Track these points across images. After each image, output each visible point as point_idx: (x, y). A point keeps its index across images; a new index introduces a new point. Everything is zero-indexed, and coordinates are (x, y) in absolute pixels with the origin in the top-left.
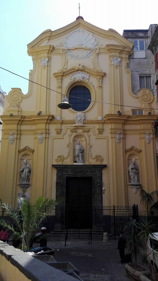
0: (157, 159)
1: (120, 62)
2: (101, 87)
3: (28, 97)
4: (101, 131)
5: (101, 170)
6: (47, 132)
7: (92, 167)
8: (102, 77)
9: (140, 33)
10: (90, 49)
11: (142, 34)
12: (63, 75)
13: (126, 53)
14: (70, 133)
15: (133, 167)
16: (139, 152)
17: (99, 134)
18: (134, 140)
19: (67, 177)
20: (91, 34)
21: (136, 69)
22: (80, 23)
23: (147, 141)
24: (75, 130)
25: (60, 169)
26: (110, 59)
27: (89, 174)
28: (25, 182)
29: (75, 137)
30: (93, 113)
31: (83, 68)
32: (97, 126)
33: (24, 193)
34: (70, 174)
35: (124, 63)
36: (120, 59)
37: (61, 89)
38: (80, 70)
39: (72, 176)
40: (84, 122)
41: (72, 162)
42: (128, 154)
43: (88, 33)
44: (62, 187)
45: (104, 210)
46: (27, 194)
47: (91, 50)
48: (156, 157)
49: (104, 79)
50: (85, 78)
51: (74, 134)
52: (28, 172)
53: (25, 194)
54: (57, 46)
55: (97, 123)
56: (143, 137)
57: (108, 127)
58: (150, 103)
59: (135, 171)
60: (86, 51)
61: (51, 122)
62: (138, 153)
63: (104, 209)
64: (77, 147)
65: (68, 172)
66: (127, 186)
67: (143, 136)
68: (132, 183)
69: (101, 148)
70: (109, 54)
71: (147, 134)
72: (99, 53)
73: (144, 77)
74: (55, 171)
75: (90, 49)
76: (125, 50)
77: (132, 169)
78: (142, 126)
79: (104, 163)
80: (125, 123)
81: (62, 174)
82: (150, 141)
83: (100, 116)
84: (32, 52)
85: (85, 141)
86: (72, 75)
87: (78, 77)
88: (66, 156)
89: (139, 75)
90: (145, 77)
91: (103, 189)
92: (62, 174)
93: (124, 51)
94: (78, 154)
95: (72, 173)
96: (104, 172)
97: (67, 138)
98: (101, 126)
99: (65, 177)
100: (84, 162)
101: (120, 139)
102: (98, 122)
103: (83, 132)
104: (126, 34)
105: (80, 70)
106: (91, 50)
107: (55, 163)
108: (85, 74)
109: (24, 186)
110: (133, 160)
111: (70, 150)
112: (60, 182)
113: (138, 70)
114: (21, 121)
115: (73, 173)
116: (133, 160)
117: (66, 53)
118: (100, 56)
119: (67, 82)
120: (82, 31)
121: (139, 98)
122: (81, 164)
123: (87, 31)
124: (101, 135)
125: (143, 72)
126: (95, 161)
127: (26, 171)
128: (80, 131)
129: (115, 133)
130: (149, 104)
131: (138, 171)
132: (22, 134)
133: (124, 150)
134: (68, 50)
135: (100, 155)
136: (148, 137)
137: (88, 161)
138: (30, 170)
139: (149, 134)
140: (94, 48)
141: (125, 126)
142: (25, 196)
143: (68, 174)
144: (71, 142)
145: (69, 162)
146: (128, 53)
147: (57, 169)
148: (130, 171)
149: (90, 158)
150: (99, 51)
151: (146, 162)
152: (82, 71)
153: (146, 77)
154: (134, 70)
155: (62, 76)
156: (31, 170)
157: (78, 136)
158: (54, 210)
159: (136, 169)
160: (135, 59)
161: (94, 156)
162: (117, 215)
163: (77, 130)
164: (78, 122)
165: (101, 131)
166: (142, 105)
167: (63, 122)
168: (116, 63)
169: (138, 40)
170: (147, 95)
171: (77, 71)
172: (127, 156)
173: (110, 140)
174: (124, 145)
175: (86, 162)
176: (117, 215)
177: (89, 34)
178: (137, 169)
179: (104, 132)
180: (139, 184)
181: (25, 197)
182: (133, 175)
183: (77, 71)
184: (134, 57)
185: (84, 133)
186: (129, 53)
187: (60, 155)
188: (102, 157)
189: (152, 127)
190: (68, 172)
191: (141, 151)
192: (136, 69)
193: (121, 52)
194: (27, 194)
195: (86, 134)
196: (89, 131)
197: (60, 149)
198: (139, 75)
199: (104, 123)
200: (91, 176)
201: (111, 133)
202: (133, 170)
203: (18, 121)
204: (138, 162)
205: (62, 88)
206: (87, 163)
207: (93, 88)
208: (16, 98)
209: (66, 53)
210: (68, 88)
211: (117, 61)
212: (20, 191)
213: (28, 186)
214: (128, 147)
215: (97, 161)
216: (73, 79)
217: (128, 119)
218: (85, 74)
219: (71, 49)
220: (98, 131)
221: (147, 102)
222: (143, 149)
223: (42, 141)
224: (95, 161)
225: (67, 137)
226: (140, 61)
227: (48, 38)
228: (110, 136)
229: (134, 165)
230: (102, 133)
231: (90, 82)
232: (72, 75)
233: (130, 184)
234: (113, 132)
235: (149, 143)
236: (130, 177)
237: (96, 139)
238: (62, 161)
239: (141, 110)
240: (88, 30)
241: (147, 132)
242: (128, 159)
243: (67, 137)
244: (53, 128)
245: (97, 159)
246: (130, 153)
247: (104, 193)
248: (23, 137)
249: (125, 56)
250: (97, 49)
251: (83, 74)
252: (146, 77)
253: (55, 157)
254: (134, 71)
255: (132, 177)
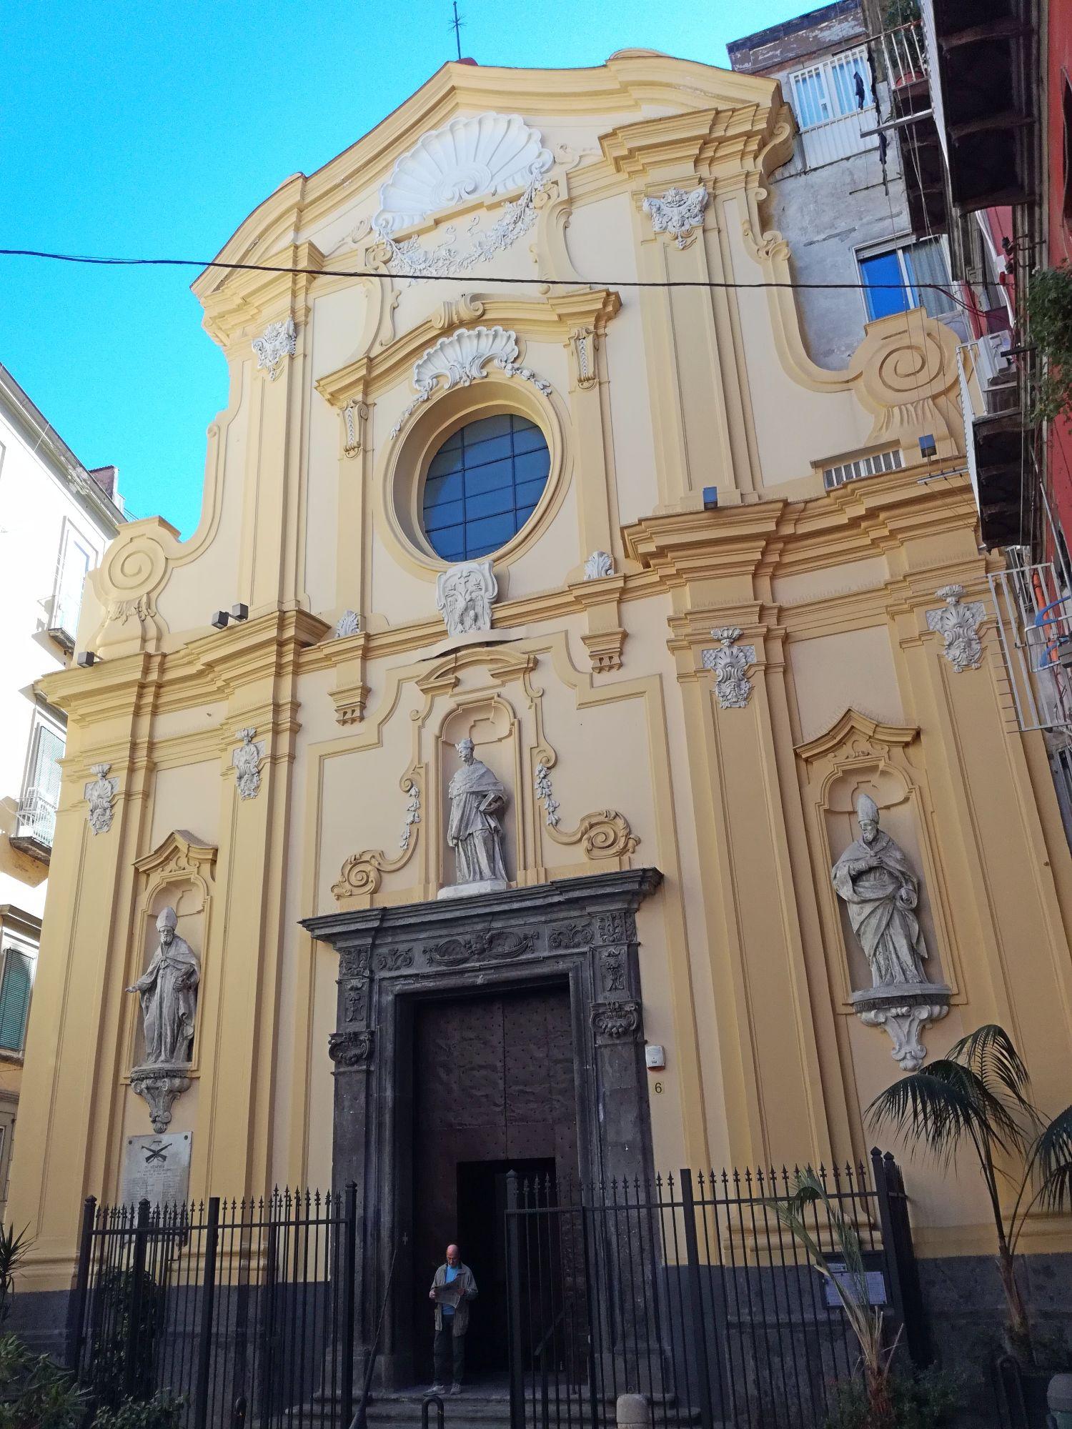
0: (1054, 773)
1: (705, 208)
2: (594, 380)
3: (195, 555)
4: (610, 653)
5: (629, 914)
6: (287, 720)
7: (556, 899)
8: (598, 319)
9: (829, 28)
10: (518, 197)
11: (845, 25)
12: (371, 374)
13: (740, 146)
14: (421, 701)
15: (862, 865)
16: (907, 745)
17: (601, 670)
18: (852, 671)
19: (401, 997)
20: (518, 119)
21: (832, 226)
22: (453, 88)
23: (955, 652)
24: (450, 679)
25: (362, 937)
26: (639, 208)
27: (544, 956)
28: (162, 1057)
29: (451, 720)
30: (559, 547)
31: (478, 304)
32: (581, 623)
33: (161, 1131)
34: (419, 968)
35: (736, 213)
36: (697, 195)
37: (361, 457)
38: (462, 324)
39: (430, 984)
40: (498, 615)
41: (433, 885)
42: (824, 769)
43: (504, 118)
44: (368, 1072)
45: (667, 1210)
46: (174, 1140)
47: (523, 201)
48: (1050, 757)
49: (615, 329)
50: (496, 362)
51: (445, 703)
52: (178, 990)
53: (166, 1139)
54: (342, 243)
55: (578, 599)
56: (692, 668)
57: (652, 616)
58: (946, 392)
59: (880, 894)
60: (498, 212)
61: (304, 659)
62: (898, 751)
63: (666, 1200)
64: (460, 783)
65: (409, 962)
66: (835, 1014)
67: (914, 622)
68: (877, 989)
69: (619, 756)
70: (639, 183)
71: (942, 599)
72: (571, 201)
73: (894, 252)
74: (330, 962)
75: (518, 197)
76: (730, 133)
77: (856, 878)
78: (905, 557)
79: (642, 860)
80: (778, 565)
81: (372, 980)
82: (976, 646)
83: (595, 554)
84: (222, 316)
85: (511, 738)
86: (419, 366)
87: (453, 363)
88: (395, 852)
89: (857, 251)
90: (900, 252)
91: (651, 1056)
92: (372, 980)
93: (722, 141)
94: (465, 822)
95: (431, 961)
96: (652, 926)
97: (405, 735)
98: (605, 617)
99: (390, 998)
100: (510, 877)
101: (745, 676)
102: (579, 597)
103: (498, 682)
104: (745, 59)
105: (462, 324)
106: (523, 201)
107: (329, 906)
108: (495, 336)
109: (149, 1082)
110: (863, 806)
111: (422, 812)
112: (356, 1034)
113: (842, 225)
114: (153, 689)
115: (439, 964)
116: (863, 806)
117: (390, 260)
118: (580, 215)
119: (398, 403)
120: (466, 125)
121: (860, 382)
122: (483, 891)
123: (493, 114)
124: (614, 675)
125: (877, 228)
126: (580, 851)
127: (167, 983)
128: (477, 678)
129: (695, 641)
130: (934, 397)
131: (919, 888)
132: (162, 766)
133: (131, 858)
134: (397, 241)
135: (614, 807)
136: (953, 620)
137: (540, 861)
138: (191, 973)
139: (959, 598)
140: (537, 185)
141: (781, 584)
142: (163, 1153)
143: (406, 977)
144: (429, 755)
145: (409, 888)
146: (753, 146)
147: (339, 950)
148: (846, 892)
149: (546, 837)
150: (569, 189)
151: (969, 808)
152: (473, 323)
153: (905, 249)
154: (818, 233)
155: (367, 384)
156: (199, 975)
157: (467, 712)
158: (322, 1227)
159: (903, 888)
160: (815, 169)
161: (572, 825)
162: (764, 1256)
163: (459, 674)
164: (462, 623)
165: (610, 653)
166: (889, 417)
167: (374, 644)
168: (676, 218)
169: (820, 66)
170: (917, 348)
171: (449, 329)
172: (815, 792)
173: (675, 691)
174: (785, 711)
175: (520, 874)
176: (764, 1256)
177: (509, 122)
178: (906, 876)
179: (632, 649)
180: (931, 989)
181: (164, 1158)
182: (874, 921)
183: (449, 329)
184: (811, 163)
185: (503, 684)
186: (763, 144)
187: (357, 852)
188: (627, 825)
189: (980, 550)
190: (409, 962)
191: (918, 735)
192: (832, 226)
193: (298, 669)
194: (174, 1140)
195: (514, 690)
196: (533, 665)
197: (372, 820)
198: (857, 251)
199: (623, 595)
200: (562, 966)
201: (673, 647)
202: (865, 883)
203: (136, 689)
204: (904, 821)
205: (365, 451)
206: (526, 878)
207: (542, 396)
208: (140, 571)
209: (390, 260)
210: (404, 436)
211: (683, 209)
212: (138, 1114)
213: (177, 1082)
214: (817, 720)
215: (596, 852)
216: (428, 381)
217: (788, 530)
218: (495, 336)
219: (411, 230)
220: (587, 651)
221: (913, 396)
222: (933, 718)
223: (255, 778)
224: (580, 851)
225: (400, 733)
226: (851, 174)
227: (293, 218)
228: (669, 664)
229: (870, 844)
230: (616, 660)
231: (526, 373)
232: (420, 362)
233: (857, 996)
234: (688, 634)
235: (973, 662)
236: (850, 937)
237: (582, 705)
238: (371, 886)
239: (881, 451)
240: (501, 110)
241: (946, 590)
242: (828, 812)
243: (400, 733)
244: (321, 688)
245: (590, 839)
246: (825, 759)
247: (658, 1087)
248: (167, 783)
249: (735, 167)
250: (556, 183)
251: (483, 339)
252: (905, 249)
253: (331, 874)
254: (822, 236)
255: (868, 943)
